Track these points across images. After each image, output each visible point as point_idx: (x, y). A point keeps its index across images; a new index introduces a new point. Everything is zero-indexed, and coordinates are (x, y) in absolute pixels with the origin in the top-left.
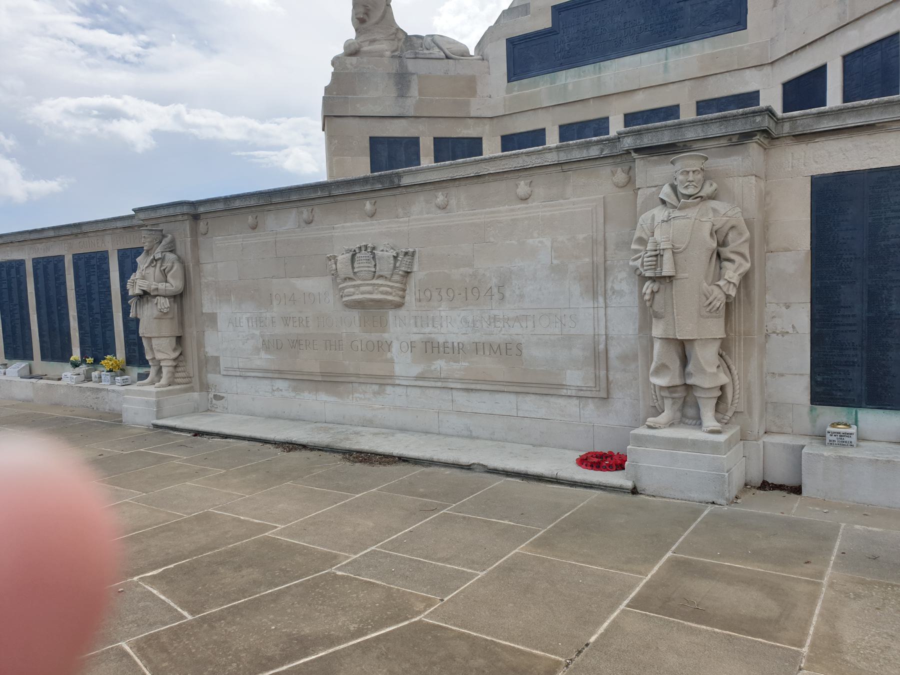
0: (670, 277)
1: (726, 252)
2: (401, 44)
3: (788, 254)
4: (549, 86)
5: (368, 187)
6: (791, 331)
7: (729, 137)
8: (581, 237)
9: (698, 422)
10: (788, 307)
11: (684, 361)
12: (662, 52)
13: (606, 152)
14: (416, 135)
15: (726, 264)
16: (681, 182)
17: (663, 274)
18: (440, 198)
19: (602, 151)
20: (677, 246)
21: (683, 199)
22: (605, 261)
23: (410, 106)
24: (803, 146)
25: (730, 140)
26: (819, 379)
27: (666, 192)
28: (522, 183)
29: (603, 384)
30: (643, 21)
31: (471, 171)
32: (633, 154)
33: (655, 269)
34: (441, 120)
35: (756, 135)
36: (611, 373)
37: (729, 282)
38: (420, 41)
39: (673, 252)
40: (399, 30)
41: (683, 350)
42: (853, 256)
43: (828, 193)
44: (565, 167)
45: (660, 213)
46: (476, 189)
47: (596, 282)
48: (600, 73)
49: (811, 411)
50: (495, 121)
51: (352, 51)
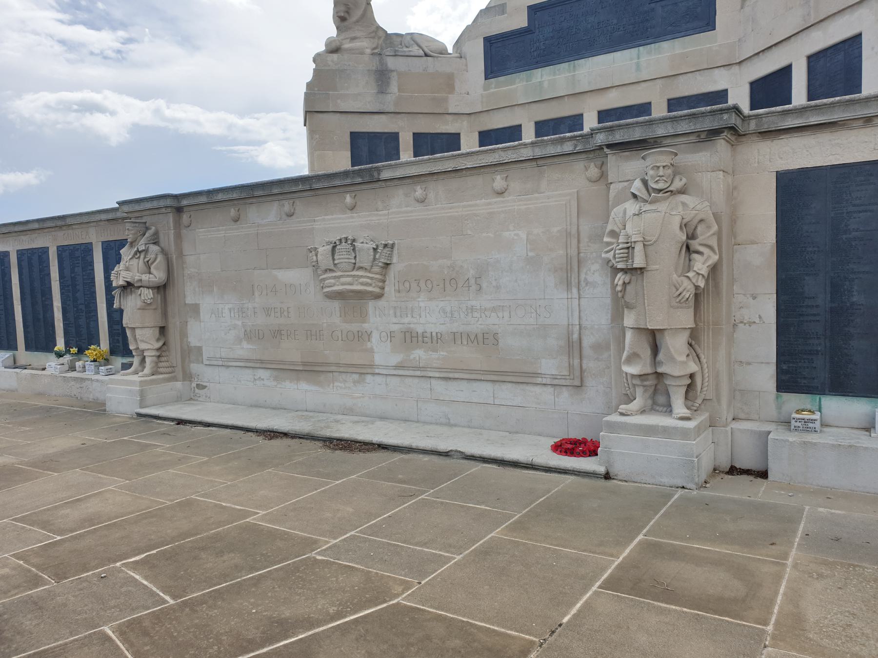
0: (641, 269)
1: (695, 244)
2: (381, 41)
3: (755, 246)
4: (525, 83)
5: (348, 181)
6: (757, 321)
7: (698, 133)
8: (555, 230)
9: (668, 409)
10: (754, 298)
11: (655, 350)
12: (634, 51)
13: (579, 148)
14: (396, 131)
15: (695, 256)
16: (652, 177)
17: (635, 266)
18: (419, 192)
19: (576, 146)
20: (648, 238)
21: (654, 193)
22: (579, 253)
23: (389, 102)
24: (768, 143)
25: (699, 136)
26: (785, 367)
27: (637, 187)
28: (498, 177)
29: (577, 373)
30: (615, 21)
31: (449, 166)
32: (606, 150)
33: (627, 261)
34: (420, 116)
35: (723, 132)
36: (585, 362)
37: (698, 274)
38: (399, 39)
39: (644, 245)
40: (379, 28)
41: (654, 339)
42: (816, 249)
43: (792, 188)
44: (541, 162)
45: (631, 207)
46: (454, 183)
47: (570, 274)
48: (574, 71)
49: (777, 398)
50: (473, 116)
51: (333, 49)
